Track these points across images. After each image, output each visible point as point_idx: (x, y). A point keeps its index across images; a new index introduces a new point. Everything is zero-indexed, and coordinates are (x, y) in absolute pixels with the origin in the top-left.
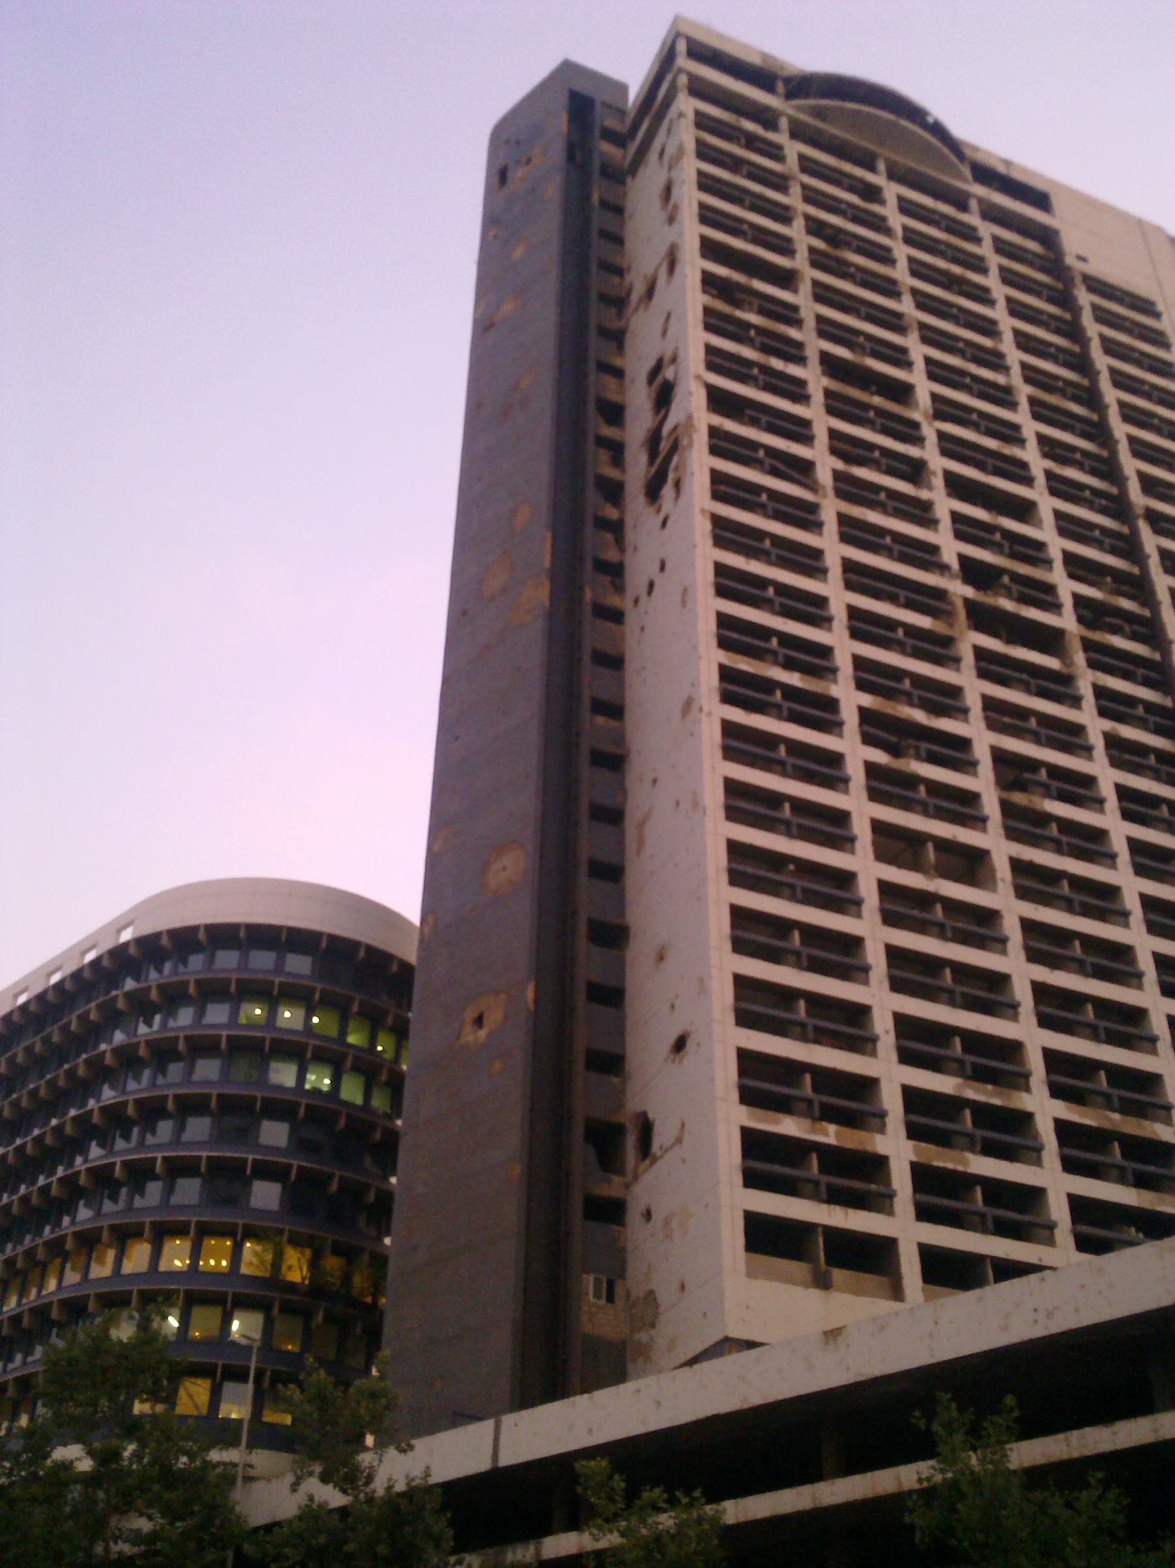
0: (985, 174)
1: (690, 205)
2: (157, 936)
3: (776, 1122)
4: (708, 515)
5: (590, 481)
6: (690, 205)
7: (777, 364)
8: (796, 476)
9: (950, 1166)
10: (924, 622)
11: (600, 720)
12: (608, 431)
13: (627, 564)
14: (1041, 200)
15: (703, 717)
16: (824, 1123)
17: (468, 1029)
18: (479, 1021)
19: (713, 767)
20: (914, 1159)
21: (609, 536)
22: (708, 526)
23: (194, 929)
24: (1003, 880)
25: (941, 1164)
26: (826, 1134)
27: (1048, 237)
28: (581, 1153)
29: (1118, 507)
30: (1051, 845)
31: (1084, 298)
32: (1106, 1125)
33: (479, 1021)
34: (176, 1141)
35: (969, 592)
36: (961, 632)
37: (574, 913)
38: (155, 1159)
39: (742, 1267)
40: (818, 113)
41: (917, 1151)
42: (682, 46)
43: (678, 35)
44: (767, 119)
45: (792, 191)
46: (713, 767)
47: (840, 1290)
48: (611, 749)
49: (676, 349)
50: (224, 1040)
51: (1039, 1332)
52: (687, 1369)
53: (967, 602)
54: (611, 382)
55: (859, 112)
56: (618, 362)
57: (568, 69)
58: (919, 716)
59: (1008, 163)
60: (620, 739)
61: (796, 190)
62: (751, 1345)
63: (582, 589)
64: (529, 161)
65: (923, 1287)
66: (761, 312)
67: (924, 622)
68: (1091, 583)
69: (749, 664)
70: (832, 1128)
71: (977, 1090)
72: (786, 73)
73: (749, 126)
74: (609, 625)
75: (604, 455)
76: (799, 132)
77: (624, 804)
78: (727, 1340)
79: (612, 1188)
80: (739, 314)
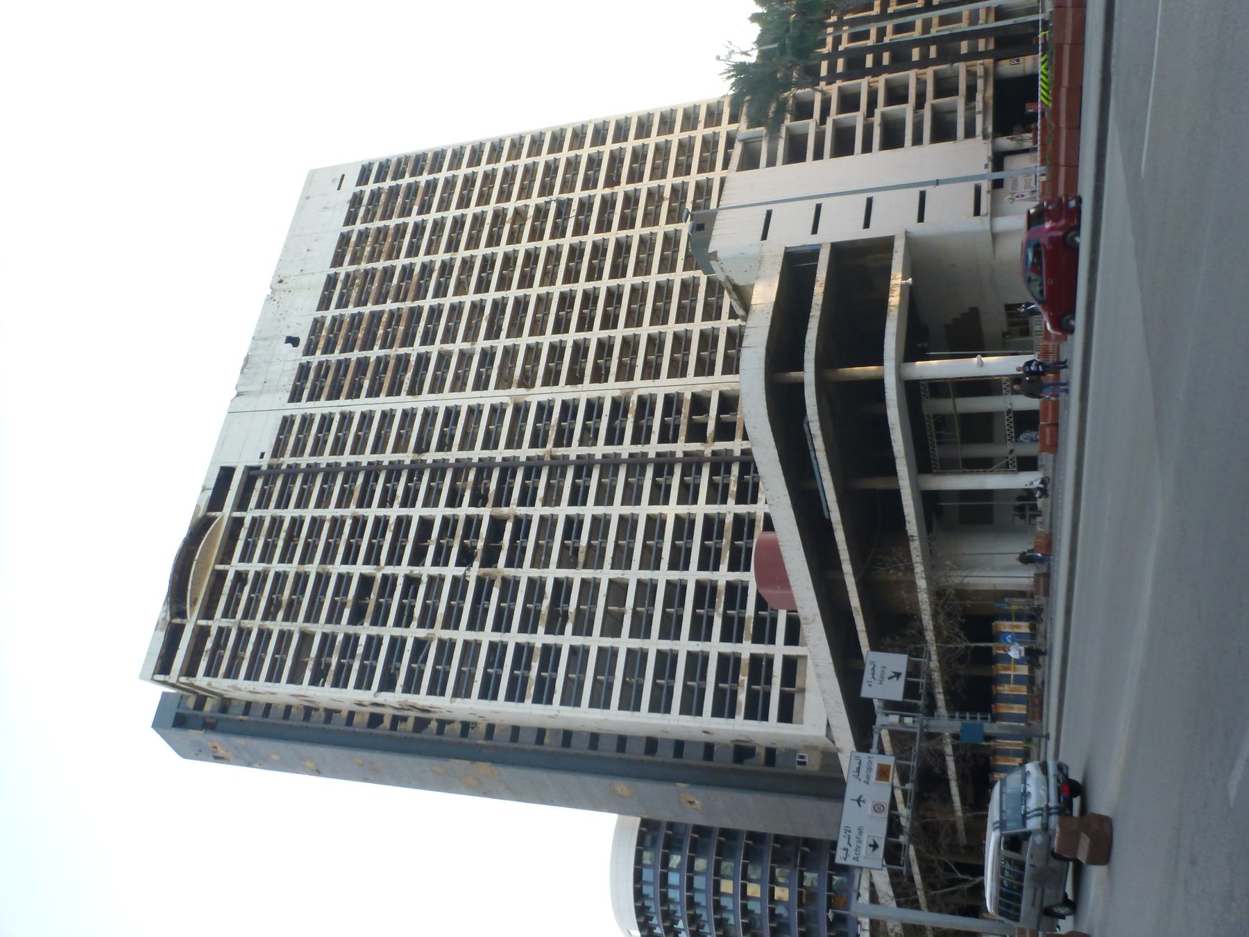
0: (216, 502)
1: (269, 687)
2: (639, 923)
3: (741, 703)
4: (453, 699)
5: (417, 735)
6: (269, 687)
7: (360, 650)
8: (426, 647)
9: (752, 625)
10: (496, 592)
11: (547, 740)
12: (387, 722)
13: (461, 720)
14: (226, 474)
15: (561, 714)
16: (739, 681)
17: (694, 806)
18: (691, 803)
19: (585, 712)
20: (750, 641)
21: (447, 727)
22: (459, 700)
23: (636, 908)
24: (622, 575)
25: (751, 629)
26: (744, 680)
27: (251, 474)
28: (748, 765)
29: (415, 471)
30: (448, 281)
31: (287, 460)
32: (728, 547)
33: (691, 803)
34: (733, 912)
35: (476, 564)
36: (499, 572)
37: (642, 760)
38: (743, 923)
39: (799, 726)
40: (194, 602)
41: (747, 640)
42: (161, 677)
43: (152, 679)
44: (202, 634)
45: (249, 626)
46: (585, 712)
47: (804, 683)
48: (560, 737)
49: (355, 704)
50: (688, 894)
51: (810, 580)
52: (836, 743)
53: (482, 566)
54: (356, 719)
55: (192, 582)
56: (345, 714)
57: (157, 725)
58: (546, 603)
59: (204, 489)
60: (555, 731)
61: (247, 623)
62: (828, 721)
63: (477, 744)
64: (216, 747)
65: (802, 646)
66: (330, 655)
67: (496, 592)
68: (462, 496)
69: (530, 688)
70: (741, 677)
71: (719, 607)
72: (168, 618)
73: (209, 645)
74: (496, 731)
75: (401, 726)
76: (208, 613)
77: (588, 732)
78: (827, 736)
79: (761, 752)
80: (333, 667)
